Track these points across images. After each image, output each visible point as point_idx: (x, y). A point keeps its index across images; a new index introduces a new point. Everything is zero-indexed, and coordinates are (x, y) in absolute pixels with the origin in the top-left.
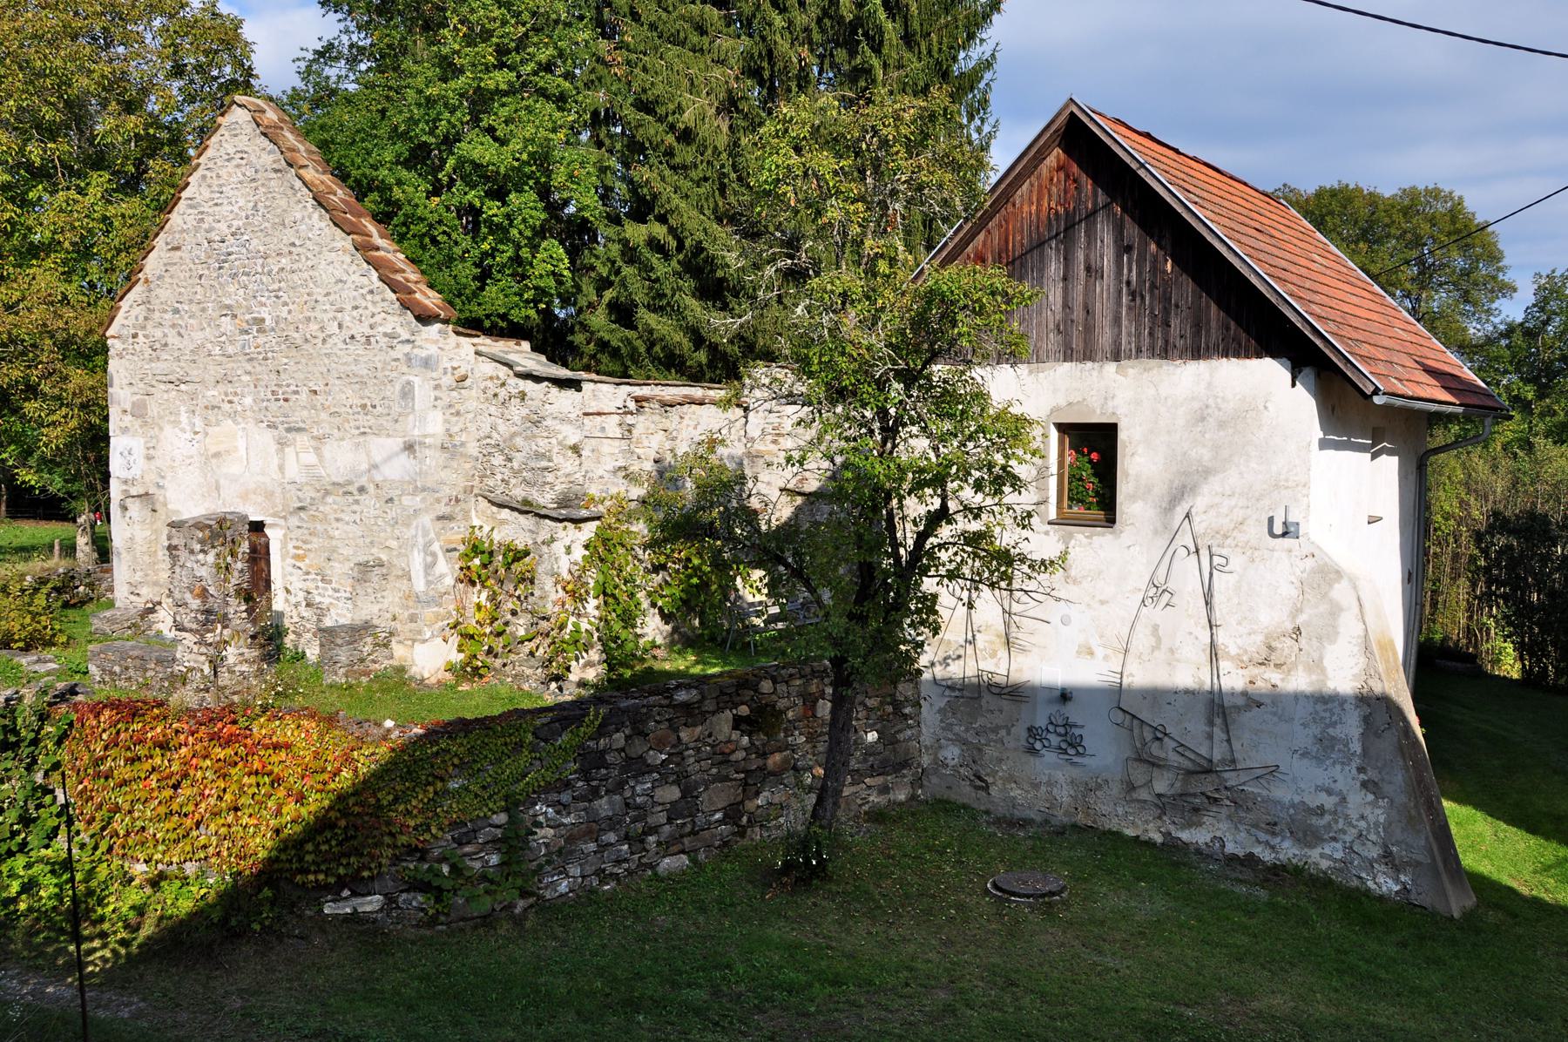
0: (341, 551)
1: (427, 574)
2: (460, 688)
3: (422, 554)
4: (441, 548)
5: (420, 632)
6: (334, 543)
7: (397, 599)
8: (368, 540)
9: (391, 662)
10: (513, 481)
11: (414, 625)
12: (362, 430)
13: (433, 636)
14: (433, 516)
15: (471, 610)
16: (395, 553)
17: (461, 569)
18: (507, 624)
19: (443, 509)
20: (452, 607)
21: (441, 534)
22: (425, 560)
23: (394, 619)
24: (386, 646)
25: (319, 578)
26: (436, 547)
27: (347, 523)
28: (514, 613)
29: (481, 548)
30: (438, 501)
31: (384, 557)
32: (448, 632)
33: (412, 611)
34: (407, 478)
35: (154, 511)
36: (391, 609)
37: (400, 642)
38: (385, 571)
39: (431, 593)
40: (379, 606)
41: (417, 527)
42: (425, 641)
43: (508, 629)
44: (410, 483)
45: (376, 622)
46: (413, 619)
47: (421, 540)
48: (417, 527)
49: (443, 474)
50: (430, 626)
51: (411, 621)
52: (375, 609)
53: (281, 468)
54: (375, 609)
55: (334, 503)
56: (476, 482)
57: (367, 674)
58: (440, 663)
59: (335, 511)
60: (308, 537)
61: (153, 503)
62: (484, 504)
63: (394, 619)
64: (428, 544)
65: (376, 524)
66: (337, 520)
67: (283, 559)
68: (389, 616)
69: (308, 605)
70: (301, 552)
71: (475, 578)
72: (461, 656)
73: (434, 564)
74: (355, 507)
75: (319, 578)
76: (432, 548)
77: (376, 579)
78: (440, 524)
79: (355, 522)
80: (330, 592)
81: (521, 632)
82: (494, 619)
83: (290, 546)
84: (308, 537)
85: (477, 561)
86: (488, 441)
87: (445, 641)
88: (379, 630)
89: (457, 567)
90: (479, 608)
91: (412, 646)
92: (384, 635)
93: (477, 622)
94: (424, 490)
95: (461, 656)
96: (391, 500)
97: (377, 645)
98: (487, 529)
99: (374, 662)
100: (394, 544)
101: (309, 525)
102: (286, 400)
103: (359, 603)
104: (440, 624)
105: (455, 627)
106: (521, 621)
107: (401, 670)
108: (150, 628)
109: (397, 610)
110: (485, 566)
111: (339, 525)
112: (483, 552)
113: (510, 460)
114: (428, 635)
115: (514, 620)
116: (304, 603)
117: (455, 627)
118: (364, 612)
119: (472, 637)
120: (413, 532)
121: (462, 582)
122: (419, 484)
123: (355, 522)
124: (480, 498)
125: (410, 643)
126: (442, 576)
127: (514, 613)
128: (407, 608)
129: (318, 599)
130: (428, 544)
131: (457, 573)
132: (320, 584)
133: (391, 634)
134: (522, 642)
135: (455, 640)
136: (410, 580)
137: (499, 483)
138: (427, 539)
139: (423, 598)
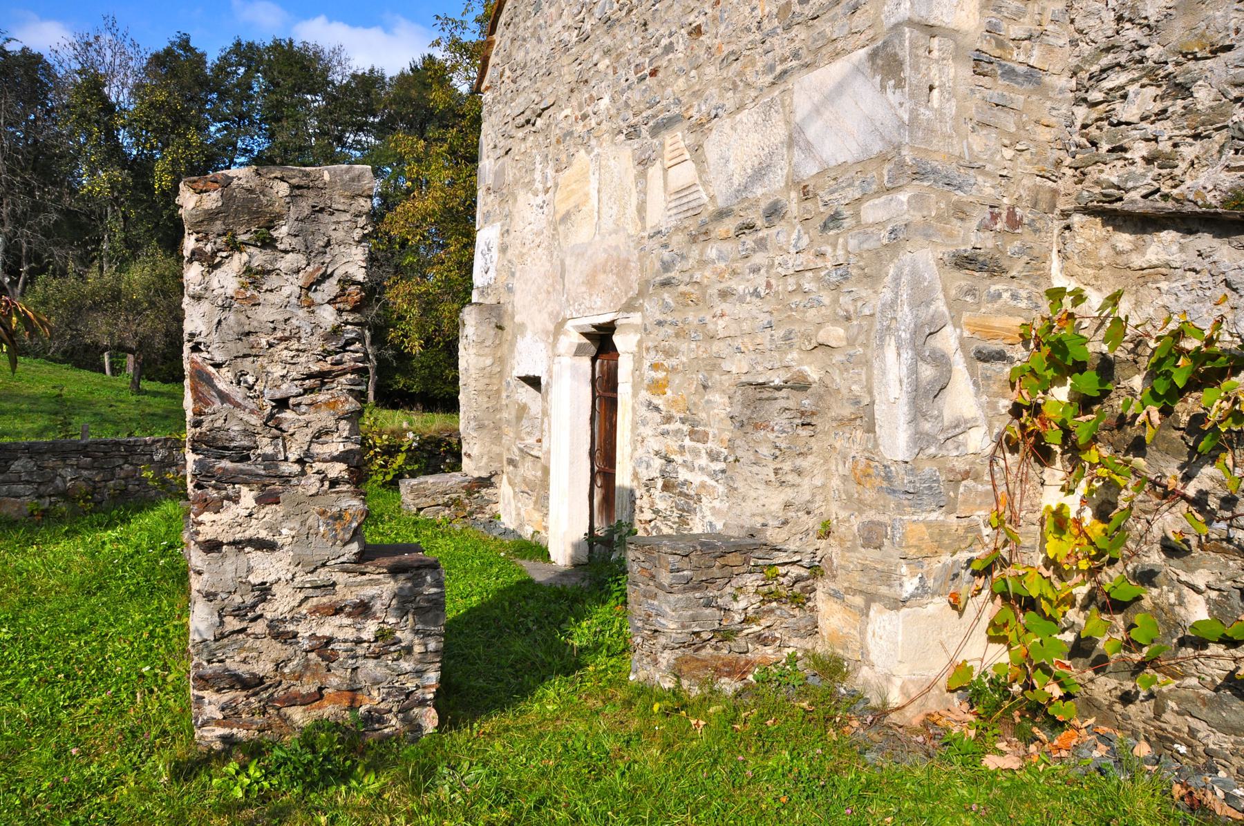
0: (726, 366)
1: (917, 414)
2: (991, 762)
3: (907, 355)
4: (963, 344)
5: (887, 577)
6: (716, 347)
7: (835, 482)
8: (779, 333)
9: (808, 644)
10: (1189, 151)
11: (872, 554)
12: (779, 69)
13: (923, 591)
14: (945, 250)
15: (1029, 534)
16: (838, 357)
17: (1016, 410)
18: (1147, 577)
19: (971, 238)
20: (981, 515)
21: (965, 306)
22: (913, 370)
23: (826, 533)
24: (800, 600)
25: (686, 428)
26: (948, 340)
27: (742, 300)
28: (1171, 549)
29: (1075, 353)
30: (961, 212)
31: (813, 373)
32: (966, 584)
33: (871, 515)
34: (877, 147)
35: (500, 328)
36: (818, 506)
37: (835, 595)
38: (807, 403)
39: (928, 469)
40: (787, 494)
41: (897, 279)
42: (898, 604)
43: (1150, 595)
44: (883, 158)
45: (773, 535)
46: (872, 537)
47: (905, 314)
48: (897, 279)
49: (978, 142)
50: (914, 563)
51: (867, 543)
52: (774, 500)
53: (641, 209)
54: (774, 500)
55: (721, 257)
56: (1066, 183)
57: (735, 669)
58: (936, 666)
59: (721, 274)
60: (674, 343)
61: (500, 316)
62: (1089, 230)
63: (826, 533)
64: (927, 331)
65: (799, 290)
66: (724, 295)
67: (635, 395)
68: (811, 522)
69: (666, 487)
70: (661, 375)
71: (1054, 439)
72: (999, 655)
73: (940, 388)
74: (759, 258)
75: (686, 428)
76: (938, 342)
77: (780, 421)
78: (962, 279)
79: (756, 293)
80: (704, 461)
81: (1197, 611)
82: (1101, 559)
83: (646, 364)
84: (674, 343)
85: (1061, 393)
86: (1107, 60)
87: (956, 606)
88: (781, 557)
89: (1005, 404)
90: (1060, 521)
91: (865, 612)
92: (795, 571)
93: (1048, 563)
94: (919, 174)
95: (999, 655)
96: (835, 218)
97: (769, 597)
98: (1095, 299)
99: (761, 640)
100: (835, 334)
101: (677, 317)
102: (653, 73)
103: (739, 484)
104: (946, 558)
105: (987, 571)
106: (1201, 578)
107: (832, 668)
108: (481, 509)
109: (835, 511)
110: (1084, 403)
111: (725, 306)
112: (1080, 367)
113: (1183, 90)
114: (910, 585)
115: (1175, 569)
116: (660, 483)
117: (987, 571)
118: (749, 507)
119: (1030, 604)
120: (887, 295)
121: (1014, 449)
122: (908, 155)
123: (756, 293)
124: (1077, 219)
125: (859, 600)
126: (961, 426)
127: (1171, 549)
128: (860, 505)
129: (683, 475)
130: (927, 331)
131: (1004, 423)
132: (687, 442)
133: (816, 571)
134: (1200, 643)
135: (985, 608)
136: (871, 429)
137: (1140, 167)
138: (925, 314)
139: (903, 480)
